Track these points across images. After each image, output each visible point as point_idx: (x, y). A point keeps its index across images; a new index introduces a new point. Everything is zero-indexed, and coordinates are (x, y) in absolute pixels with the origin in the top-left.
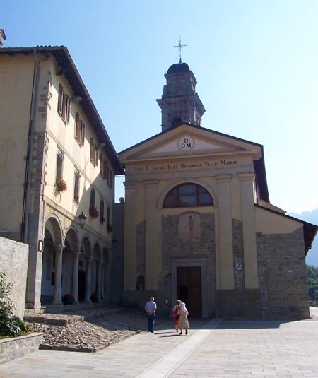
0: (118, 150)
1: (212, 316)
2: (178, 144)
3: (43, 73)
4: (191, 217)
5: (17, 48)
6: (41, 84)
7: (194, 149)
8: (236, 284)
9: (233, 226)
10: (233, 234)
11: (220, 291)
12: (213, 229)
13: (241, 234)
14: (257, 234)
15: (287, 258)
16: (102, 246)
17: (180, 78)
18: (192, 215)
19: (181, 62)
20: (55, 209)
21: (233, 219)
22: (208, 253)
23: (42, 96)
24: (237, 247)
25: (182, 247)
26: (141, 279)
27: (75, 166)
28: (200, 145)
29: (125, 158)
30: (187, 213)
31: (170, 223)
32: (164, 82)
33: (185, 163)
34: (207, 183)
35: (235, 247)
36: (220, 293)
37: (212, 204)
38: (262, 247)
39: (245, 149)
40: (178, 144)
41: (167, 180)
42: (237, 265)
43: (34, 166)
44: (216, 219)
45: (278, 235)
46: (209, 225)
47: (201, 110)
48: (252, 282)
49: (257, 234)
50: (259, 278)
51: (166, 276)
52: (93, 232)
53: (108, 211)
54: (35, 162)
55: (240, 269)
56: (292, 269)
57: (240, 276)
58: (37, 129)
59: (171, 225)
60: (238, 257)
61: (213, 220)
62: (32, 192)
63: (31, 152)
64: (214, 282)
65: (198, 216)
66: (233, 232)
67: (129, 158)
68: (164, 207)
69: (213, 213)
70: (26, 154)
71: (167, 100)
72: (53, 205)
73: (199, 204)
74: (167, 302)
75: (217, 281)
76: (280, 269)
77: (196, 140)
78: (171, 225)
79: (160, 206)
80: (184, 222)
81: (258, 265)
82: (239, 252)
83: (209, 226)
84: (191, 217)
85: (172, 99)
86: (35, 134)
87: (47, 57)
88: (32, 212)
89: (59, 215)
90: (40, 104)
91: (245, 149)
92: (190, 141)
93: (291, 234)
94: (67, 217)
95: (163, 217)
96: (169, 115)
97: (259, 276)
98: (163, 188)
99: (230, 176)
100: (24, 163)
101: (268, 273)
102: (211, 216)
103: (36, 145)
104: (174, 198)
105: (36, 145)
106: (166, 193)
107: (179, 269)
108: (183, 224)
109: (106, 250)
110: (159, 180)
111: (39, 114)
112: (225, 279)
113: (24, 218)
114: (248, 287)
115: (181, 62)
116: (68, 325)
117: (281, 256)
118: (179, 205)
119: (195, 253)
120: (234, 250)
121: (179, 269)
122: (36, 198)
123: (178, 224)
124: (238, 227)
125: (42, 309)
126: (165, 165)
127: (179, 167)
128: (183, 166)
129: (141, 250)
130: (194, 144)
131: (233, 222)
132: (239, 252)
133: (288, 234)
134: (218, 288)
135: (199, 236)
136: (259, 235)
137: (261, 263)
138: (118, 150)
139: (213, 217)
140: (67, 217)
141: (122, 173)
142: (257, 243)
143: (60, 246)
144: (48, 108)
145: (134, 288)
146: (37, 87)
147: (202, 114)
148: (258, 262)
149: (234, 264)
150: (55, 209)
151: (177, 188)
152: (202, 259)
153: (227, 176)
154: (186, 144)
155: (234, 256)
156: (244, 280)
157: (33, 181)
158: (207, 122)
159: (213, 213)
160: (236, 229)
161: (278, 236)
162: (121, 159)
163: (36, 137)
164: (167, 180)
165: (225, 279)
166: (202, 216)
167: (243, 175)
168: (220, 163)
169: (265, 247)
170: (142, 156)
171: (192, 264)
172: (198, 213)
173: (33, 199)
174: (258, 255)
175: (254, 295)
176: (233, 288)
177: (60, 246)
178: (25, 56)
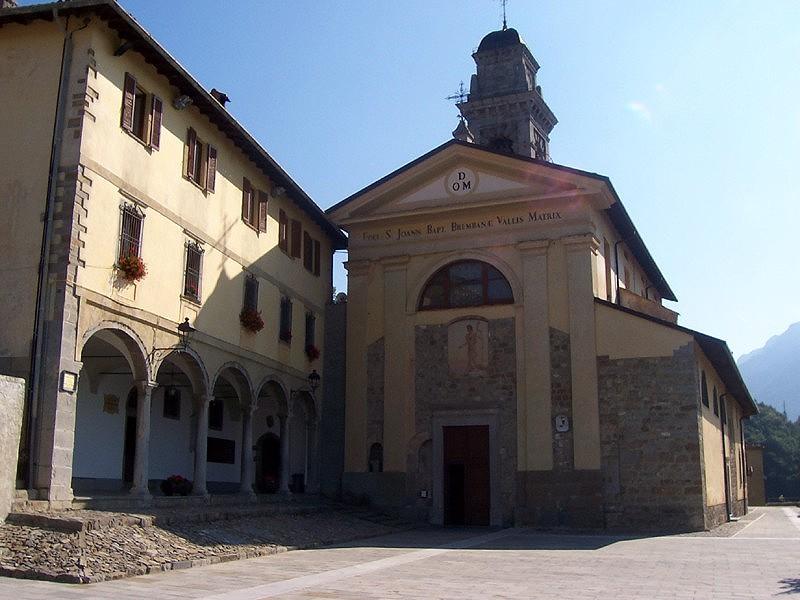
0: (324, 206)
1: (509, 523)
2: (446, 182)
3: (79, 54)
4: (470, 328)
5: (39, 6)
6: (75, 73)
7: (477, 192)
8: (556, 459)
9: (551, 343)
10: (553, 360)
11: (525, 473)
12: (512, 351)
13: (568, 360)
15: (659, 408)
16: (288, 385)
17: (503, 58)
18: (473, 324)
19: (505, 27)
20: (120, 314)
21: (552, 331)
23: (75, 96)
24: (559, 385)
25: (453, 386)
26: (376, 450)
27: (185, 231)
29: (347, 215)
30: (463, 319)
31: (431, 341)
32: (472, 68)
33: (459, 221)
34: (500, 257)
35: (555, 385)
36: (525, 477)
37: (510, 301)
38: (609, 383)
40: (446, 182)
41: (425, 255)
42: (559, 421)
43: (59, 231)
44: (519, 330)
45: (641, 360)
46: (504, 344)
47: (547, 121)
48: (588, 456)
50: (602, 448)
51: (424, 444)
52: (256, 359)
53: (310, 321)
54: (59, 224)
55: (565, 428)
56: (670, 428)
57: (564, 446)
58: (65, 161)
59: (433, 343)
60: (562, 405)
61: (513, 331)
62: (51, 281)
63: (52, 204)
65: (484, 325)
67: (353, 215)
68: (421, 308)
69: (514, 318)
70: (43, 209)
71: (477, 103)
72: (110, 304)
73: (487, 301)
74: (424, 494)
75: (520, 453)
76: (645, 429)
78: (433, 343)
79: (412, 307)
80: (458, 335)
81: (601, 422)
82: (562, 395)
83: (505, 345)
85: (484, 101)
86: (60, 170)
87: (87, 21)
88: (51, 317)
89: (135, 325)
90: (71, 113)
92: (470, 176)
93: (668, 358)
94: (161, 328)
95: (417, 328)
96: (482, 133)
97: (603, 443)
98: (421, 270)
99: (546, 243)
100: (41, 226)
101: (622, 437)
102: (509, 324)
103: (61, 192)
104: (443, 288)
105: (61, 192)
106: (424, 280)
107: (449, 431)
108: (456, 347)
109: (305, 396)
111: (68, 132)
112: (535, 451)
113: (36, 331)
114: (578, 466)
115: (505, 27)
116: (82, 534)
117: (646, 402)
118: (445, 304)
119: (478, 399)
120: (553, 392)
121: (449, 431)
122: (59, 291)
123: (446, 341)
124: (561, 345)
125: (74, 501)
126: (423, 226)
127: (448, 229)
128: (454, 227)
130: (477, 180)
131: (551, 336)
132: (562, 395)
133: (663, 358)
134: (521, 468)
135: (486, 364)
136: (603, 361)
138: (324, 206)
139: (513, 326)
140: (161, 328)
141: (342, 244)
142: (600, 377)
143: (144, 383)
144: (86, 120)
145: (362, 468)
146: (67, 80)
147: (551, 128)
148: (601, 416)
149: (553, 420)
150: (120, 314)
151: (444, 271)
152: (491, 411)
153: (538, 244)
154: (461, 183)
156: (572, 451)
157: (55, 259)
158: (565, 149)
159: (514, 318)
160: (557, 347)
161: (642, 363)
162: (335, 221)
163: (62, 176)
164: (425, 255)
165: (535, 451)
166: (492, 325)
167: (571, 240)
168: (526, 217)
169: (614, 384)
170: (377, 211)
171: (473, 420)
172: (483, 319)
173: (54, 290)
174: (601, 401)
175: (592, 482)
176: (550, 468)
177: (144, 383)
178: (22, 26)
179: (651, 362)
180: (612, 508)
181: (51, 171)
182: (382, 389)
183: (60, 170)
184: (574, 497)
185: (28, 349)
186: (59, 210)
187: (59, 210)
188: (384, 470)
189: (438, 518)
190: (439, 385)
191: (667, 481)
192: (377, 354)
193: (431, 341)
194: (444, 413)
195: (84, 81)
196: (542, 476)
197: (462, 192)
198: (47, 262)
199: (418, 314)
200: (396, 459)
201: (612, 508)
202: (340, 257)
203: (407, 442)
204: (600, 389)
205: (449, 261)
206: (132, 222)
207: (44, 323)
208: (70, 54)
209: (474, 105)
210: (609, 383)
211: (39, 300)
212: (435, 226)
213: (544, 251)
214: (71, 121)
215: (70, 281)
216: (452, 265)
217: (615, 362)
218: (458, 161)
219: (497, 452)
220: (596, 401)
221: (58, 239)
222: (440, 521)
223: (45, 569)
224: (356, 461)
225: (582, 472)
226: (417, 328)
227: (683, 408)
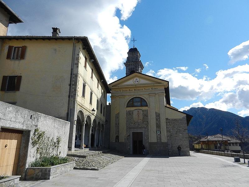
3: (77, 48)
4: (138, 111)
8: (157, 140)
10: (156, 119)
11: (151, 142)
13: (160, 119)
15: (179, 129)
20: (82, 107)
23: (77, 58)
26: (117, 137)
30: (137, 109)
31: (129, 114)
33: (136, 89)
34: (145, 97)
35: (157, 124)
37: (147, 106)
43: (73, 88)
45: (175, 119)
46: (146, 115)
48: (164, 140)
56: (182, 134)
58: (75, 72)
59: (130, 114)
63: (72, 82)
67: (113, 86)
73: (142, 106)
76: (176, 134)
80: (135, 113)
82: (158, 126)
86: (74, 74)
90: (76, 62)
93: (181, 119)
98: (128, 98)
100: (69, 87)
102: (147, 111)
103: (74, 79)
104: (131, 103)
105: (74, 79)
109: (103, 125)
111: (75, 66)
112: (153, 138)
113: (68, 110)
114: (162, 141)
119: (140, 126)
124: (158, 116)
126: (128, 90)
128: (135, 90)
129: (117, 125)
132: (158, 126)
133: (180, 119)
136: (167, 119)
139: (148, 111)
145: (114, 141)
149: (157, 131)
150: (82, 107)
152: (143, 129)
161: (175, 120)
163: (74, 76)
165: (153, 138)
166: (143, 111)
167: (160, 94)
170: (118, 86)
172: (141, 110)
175: (166, 144)
179: (177, 120)
180: (170, 150)
181: (71, 74)
183: (74, 74)
184: (162, 148)
185: (66, 115)
186: (73, 83)
187: (73, 83)
188: (119, 141)
189: (131, 153)
192: (117, 116)
193: (129, 114)
194: (133, 129)
195: (79, 55)
196: (154, 143)
197: (136, 83)
198: (71, 95)
199: (127, 108)
200: (122, 139)
201: (170, 150)
202: (196, 99)
203: (124, 135)
204: (166, 125)
205: (134, 97)
206: (84, 86)
207: (71, 109)
208: (75, 48)
209: (127, 64)
210: (168, 124)
211: (69, 104)
212: (131, 89)
213: (154, 96)
214: (76, 63)
215: (76, 100)
216: (134, 98)
217: (169, 119)
219: (144, 138)
220: (166, 127)
221: (73, 90)
222: (132, 153)
223: (89, 168)
224: (113, 140)
225: (163, 143)
226: (127, 111)
227: (184, 130)
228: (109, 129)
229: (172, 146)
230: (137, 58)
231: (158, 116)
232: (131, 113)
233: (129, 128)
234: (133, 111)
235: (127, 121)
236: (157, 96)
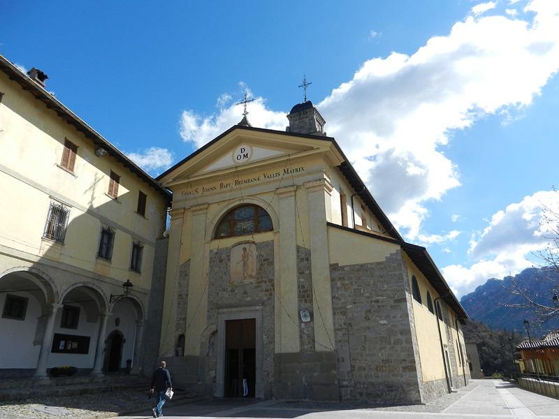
12: (272, 263)
14: (331, 266)
18: (247, 246)
22: (265, 298)
24: (303, 287)
25: (232, 291)
28: (259, 153)
31: (220, 259)
33: (240, 179)
39: (312, 149)
48: (325, 341)
49: (331, 266)
57: (307, 336)
64: (272, 342)
66: (298, 265)
67: (174, 180)
77: (253, 148)
78: (221, 261)
80: (237, 255)
82: (306, 294)
84: (245, 249)
91: (312, 149)
98: (216, 212)
102: (270, 245)
107: (228, 323)
110: (209, 204)
114: (318, 348)
123: (229, 259)
124: (304, 257)
129: (183, 299)
135: (254, 274)
136: (334, 267)
137: (338, 310)
142: (332, 280)
152: (257, 308)
155: (300, 301)
174: (333, 297)
176: (298, 350)
180: (345, 383)
182: (187, 295)
184: (316, 374)
188: (185, 354)
190: (224, 290)
191: (387, 361)
197: (243, 160)
200: (194, 347)
218: (240, 141)
228: (158, 312)
229: (353, 367)
230: (311, 125)
231: (304, 257)
232: (223, 257)
233: (216, 307)
234: (229, 250)
235: (212, 284)
236: (301, 193)
